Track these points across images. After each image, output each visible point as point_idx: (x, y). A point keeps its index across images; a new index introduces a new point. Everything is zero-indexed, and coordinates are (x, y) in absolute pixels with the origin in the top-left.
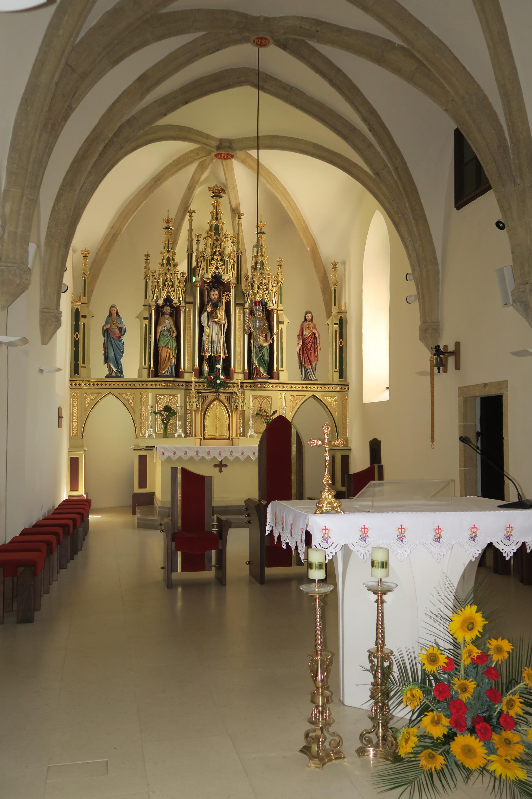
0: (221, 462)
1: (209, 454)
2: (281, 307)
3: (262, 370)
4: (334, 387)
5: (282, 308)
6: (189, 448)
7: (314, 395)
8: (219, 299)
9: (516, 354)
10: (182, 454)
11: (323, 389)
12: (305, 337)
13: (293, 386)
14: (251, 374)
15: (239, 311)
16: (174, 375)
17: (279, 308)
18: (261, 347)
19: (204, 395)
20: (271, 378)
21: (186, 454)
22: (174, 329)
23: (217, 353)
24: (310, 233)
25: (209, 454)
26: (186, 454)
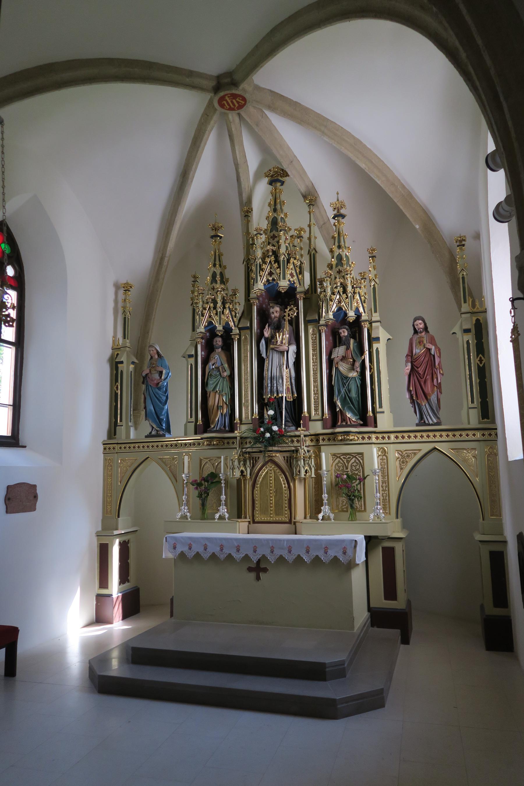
0: (259, 562)
1: (238, 550)
2: (376, 317)
3: (349, 415)
4: (470, 433)
5: (378, 319)
7: (435, 448)
8: (282, 318)
10: (201, 550)
11: (451, 438)
12: (416, 357)
13: (400, 435)
14: (335, 418)
15: (313, 331)
16: (227, 429)
17: (373, 319)
18: (345, 379)
19: (255, 455)
20: (365, 424)
21: (205, 549)
22: (226, 366)
23: (278, 394)
24: (417, 203)
25: (238, 550)
26: (205, 549)
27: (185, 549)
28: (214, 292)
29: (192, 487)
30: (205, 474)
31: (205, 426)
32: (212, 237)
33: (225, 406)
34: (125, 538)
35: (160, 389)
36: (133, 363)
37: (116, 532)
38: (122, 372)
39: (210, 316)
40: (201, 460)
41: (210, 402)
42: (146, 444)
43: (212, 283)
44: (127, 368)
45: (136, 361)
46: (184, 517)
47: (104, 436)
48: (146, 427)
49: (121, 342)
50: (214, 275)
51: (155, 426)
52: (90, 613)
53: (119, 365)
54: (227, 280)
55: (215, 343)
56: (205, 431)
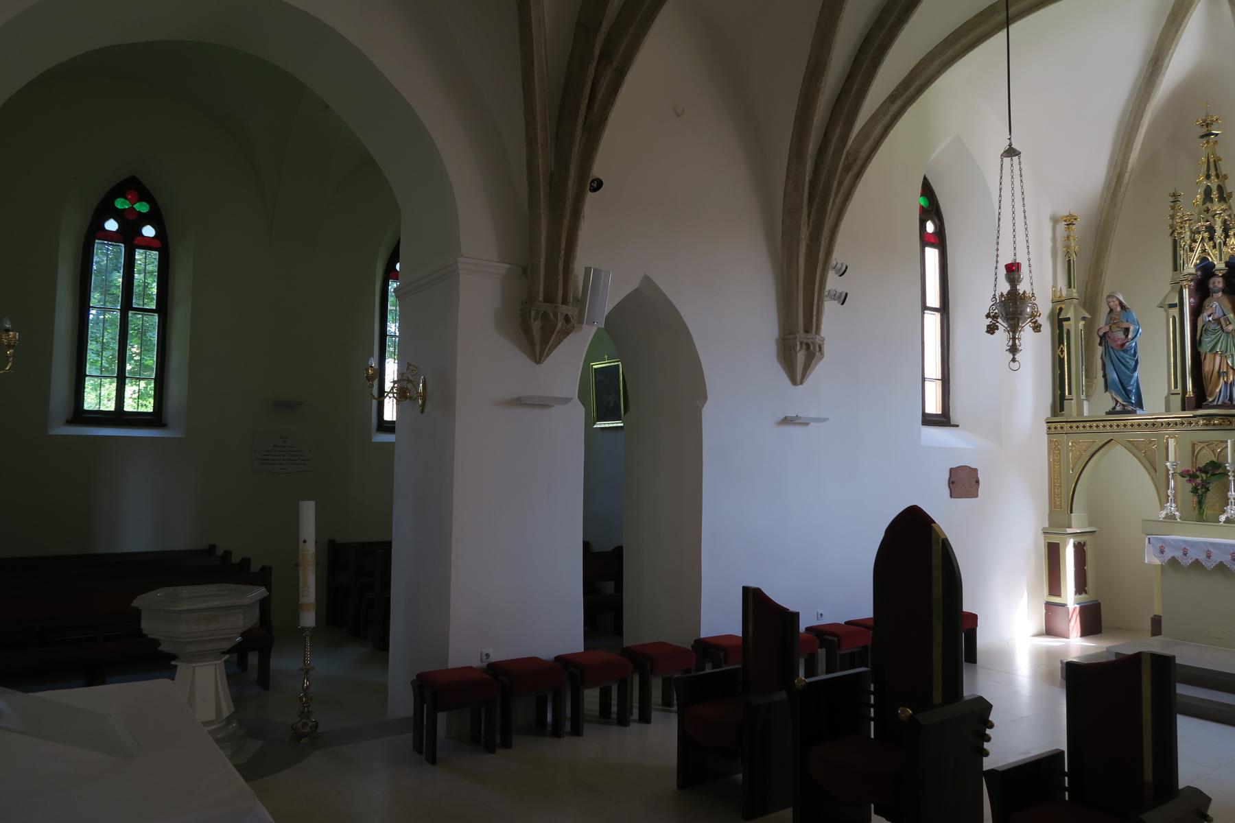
6: (1192, 544)
9: (422, 412)
10: (1202, 557)
26: (1209, 557)
27: (1178, 554)
28: (1209, 216)
29: (1179, 477)
30: (1202, 463)
31: (1200, 398)
32: (1202, 137)
33: (1231, 372)
34: (1081, 539)
35: (1125, 351)
36: (1084, 318)
37: (1069, 531)
38: (1068, 331)
39: (1204, 251)
40: (1194, 445)
41: (1207, 367)
42: (1108, 423)
43: (1204, 203)
44: (1075, 326)
45: (1088, 316)
46: (1171, 517)
47: (1047, 413)
48: (1104, 401)
49: (1064, 294)
50: (1208, 192)
51: (1120, 400)
52: (1037, 620)
53: (1065, 323)
54: (1230, 195)
55: (1211, 286)
56: (1199, 406)
